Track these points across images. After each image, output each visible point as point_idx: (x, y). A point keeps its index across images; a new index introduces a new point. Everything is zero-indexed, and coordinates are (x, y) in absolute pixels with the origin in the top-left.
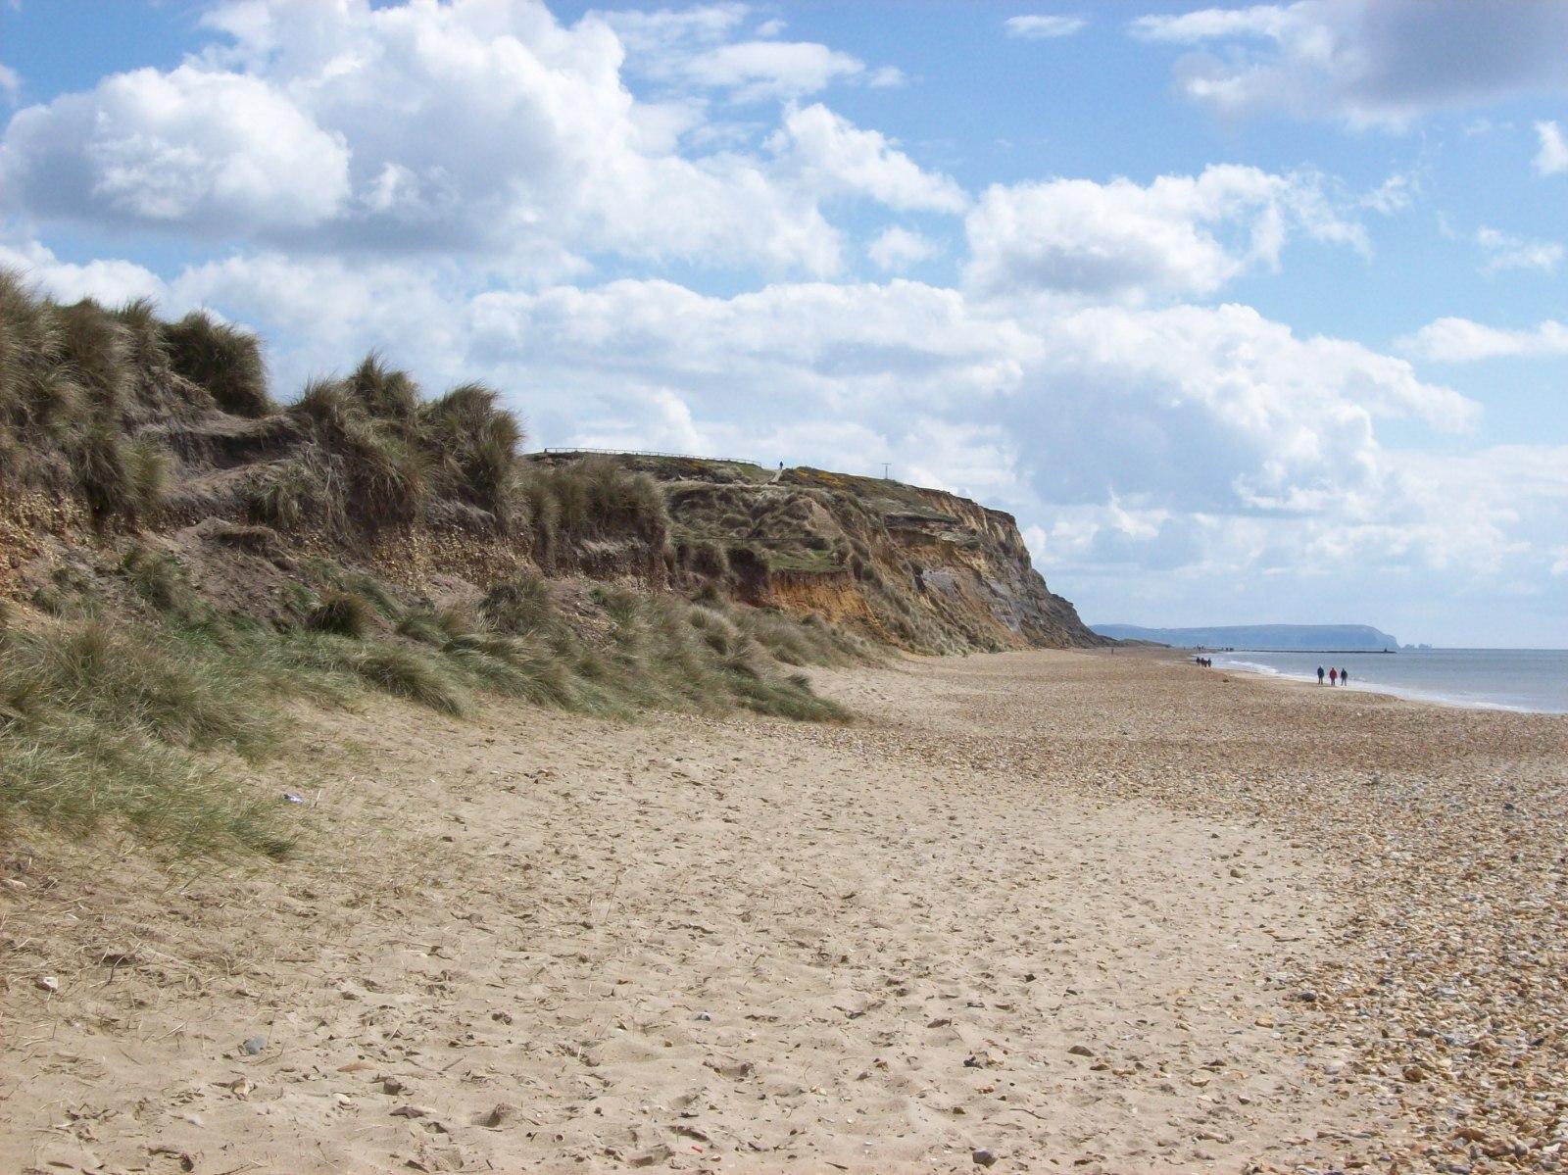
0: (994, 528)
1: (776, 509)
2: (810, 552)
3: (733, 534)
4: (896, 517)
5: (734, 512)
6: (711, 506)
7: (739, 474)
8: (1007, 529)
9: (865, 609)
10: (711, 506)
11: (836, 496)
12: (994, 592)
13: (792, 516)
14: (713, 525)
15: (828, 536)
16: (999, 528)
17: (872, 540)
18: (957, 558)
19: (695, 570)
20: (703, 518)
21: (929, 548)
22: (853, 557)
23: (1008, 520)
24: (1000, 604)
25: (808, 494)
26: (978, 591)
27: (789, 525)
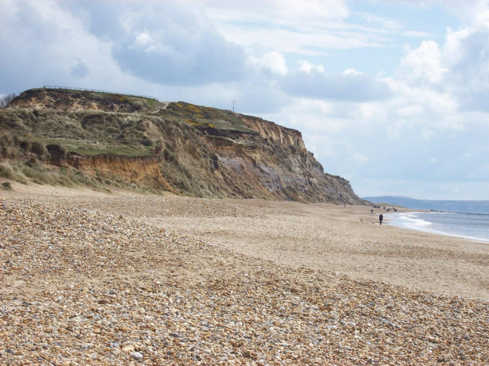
0: (288, 139)
1: (133, 125)
2: (143, 147)
3: (110, 136)
4: (226, 131)
5: (113, 126)
6: (102, 122)
7: (145, 104)
8: (296, 138)
9: (158, 173)
10: (102, 122)
11: (166, 120)
12: (262, 171)
13: (139, 129)
14: (103, 132)
15: (153, 140)
16: (291, 138)
17: (184, 143)
18: (244, 153)
19: (32, 152)
20: (98, 128)
21: (228, 147)
22: (165, 150)
23: (298, 134)
24: (265, 177)
25: (149, 119)
26: (253, 170)
27: (136, 133)
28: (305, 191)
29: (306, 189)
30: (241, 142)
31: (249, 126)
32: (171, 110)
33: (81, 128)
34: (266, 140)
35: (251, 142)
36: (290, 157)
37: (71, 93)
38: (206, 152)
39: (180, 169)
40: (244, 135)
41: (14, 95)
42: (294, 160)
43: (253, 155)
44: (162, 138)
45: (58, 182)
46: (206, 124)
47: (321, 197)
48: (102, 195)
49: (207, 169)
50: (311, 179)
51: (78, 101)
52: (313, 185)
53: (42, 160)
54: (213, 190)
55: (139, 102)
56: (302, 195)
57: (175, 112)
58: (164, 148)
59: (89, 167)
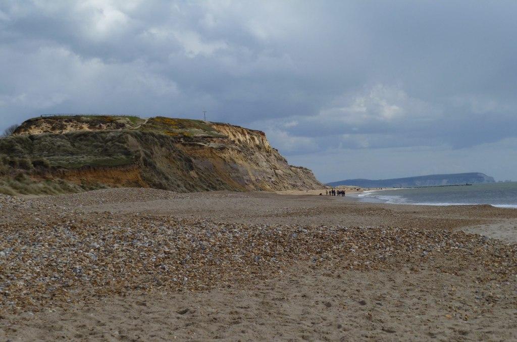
0: (253, 139)
7: (128, 122)
11: (143, 133)
20: (85, 145)
22: (143, 158)
28: (272, 182)
29: (273, 180)
30: (212, 145)
31: (219, 131)
32: (150, 124)
33: (71, 146)
34: (234, 141)
35: (221, 145)
36: (257, 154)
37: (65, 118)
38: (181, 157)
39: (158, 172)
40: (214, 139)
41: (17, 125)
42: (260, 156)
43: (223, 155)
44: (140, 148)
45: (42, 191)
46: (181, 133)
47: (286, 185)
48: (37, 197)
49: (183, 171)
50: (276, 171)
51: (70, 125)
52: (278, 176)
53: (30, 175)
54: (189, 188)
55: (122, 121)
56: (269, 186)
57: (154, 125)
58: (143, 155)
59: (75, 177)
